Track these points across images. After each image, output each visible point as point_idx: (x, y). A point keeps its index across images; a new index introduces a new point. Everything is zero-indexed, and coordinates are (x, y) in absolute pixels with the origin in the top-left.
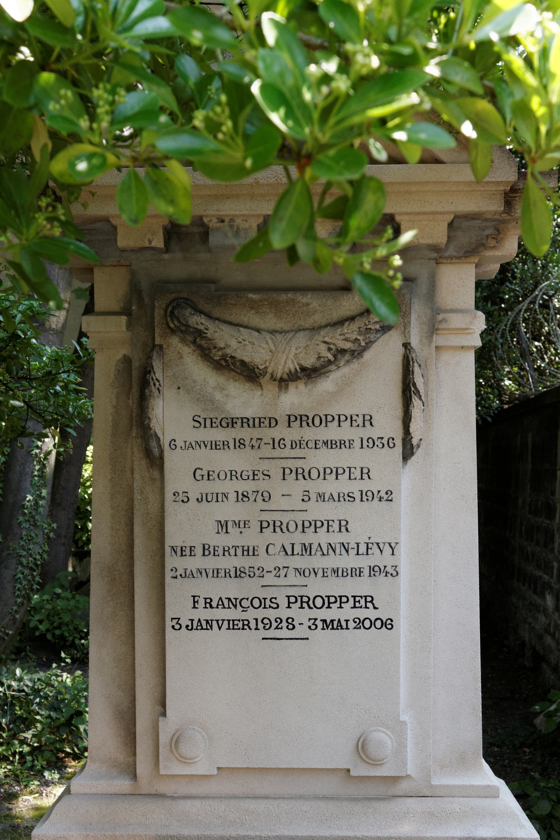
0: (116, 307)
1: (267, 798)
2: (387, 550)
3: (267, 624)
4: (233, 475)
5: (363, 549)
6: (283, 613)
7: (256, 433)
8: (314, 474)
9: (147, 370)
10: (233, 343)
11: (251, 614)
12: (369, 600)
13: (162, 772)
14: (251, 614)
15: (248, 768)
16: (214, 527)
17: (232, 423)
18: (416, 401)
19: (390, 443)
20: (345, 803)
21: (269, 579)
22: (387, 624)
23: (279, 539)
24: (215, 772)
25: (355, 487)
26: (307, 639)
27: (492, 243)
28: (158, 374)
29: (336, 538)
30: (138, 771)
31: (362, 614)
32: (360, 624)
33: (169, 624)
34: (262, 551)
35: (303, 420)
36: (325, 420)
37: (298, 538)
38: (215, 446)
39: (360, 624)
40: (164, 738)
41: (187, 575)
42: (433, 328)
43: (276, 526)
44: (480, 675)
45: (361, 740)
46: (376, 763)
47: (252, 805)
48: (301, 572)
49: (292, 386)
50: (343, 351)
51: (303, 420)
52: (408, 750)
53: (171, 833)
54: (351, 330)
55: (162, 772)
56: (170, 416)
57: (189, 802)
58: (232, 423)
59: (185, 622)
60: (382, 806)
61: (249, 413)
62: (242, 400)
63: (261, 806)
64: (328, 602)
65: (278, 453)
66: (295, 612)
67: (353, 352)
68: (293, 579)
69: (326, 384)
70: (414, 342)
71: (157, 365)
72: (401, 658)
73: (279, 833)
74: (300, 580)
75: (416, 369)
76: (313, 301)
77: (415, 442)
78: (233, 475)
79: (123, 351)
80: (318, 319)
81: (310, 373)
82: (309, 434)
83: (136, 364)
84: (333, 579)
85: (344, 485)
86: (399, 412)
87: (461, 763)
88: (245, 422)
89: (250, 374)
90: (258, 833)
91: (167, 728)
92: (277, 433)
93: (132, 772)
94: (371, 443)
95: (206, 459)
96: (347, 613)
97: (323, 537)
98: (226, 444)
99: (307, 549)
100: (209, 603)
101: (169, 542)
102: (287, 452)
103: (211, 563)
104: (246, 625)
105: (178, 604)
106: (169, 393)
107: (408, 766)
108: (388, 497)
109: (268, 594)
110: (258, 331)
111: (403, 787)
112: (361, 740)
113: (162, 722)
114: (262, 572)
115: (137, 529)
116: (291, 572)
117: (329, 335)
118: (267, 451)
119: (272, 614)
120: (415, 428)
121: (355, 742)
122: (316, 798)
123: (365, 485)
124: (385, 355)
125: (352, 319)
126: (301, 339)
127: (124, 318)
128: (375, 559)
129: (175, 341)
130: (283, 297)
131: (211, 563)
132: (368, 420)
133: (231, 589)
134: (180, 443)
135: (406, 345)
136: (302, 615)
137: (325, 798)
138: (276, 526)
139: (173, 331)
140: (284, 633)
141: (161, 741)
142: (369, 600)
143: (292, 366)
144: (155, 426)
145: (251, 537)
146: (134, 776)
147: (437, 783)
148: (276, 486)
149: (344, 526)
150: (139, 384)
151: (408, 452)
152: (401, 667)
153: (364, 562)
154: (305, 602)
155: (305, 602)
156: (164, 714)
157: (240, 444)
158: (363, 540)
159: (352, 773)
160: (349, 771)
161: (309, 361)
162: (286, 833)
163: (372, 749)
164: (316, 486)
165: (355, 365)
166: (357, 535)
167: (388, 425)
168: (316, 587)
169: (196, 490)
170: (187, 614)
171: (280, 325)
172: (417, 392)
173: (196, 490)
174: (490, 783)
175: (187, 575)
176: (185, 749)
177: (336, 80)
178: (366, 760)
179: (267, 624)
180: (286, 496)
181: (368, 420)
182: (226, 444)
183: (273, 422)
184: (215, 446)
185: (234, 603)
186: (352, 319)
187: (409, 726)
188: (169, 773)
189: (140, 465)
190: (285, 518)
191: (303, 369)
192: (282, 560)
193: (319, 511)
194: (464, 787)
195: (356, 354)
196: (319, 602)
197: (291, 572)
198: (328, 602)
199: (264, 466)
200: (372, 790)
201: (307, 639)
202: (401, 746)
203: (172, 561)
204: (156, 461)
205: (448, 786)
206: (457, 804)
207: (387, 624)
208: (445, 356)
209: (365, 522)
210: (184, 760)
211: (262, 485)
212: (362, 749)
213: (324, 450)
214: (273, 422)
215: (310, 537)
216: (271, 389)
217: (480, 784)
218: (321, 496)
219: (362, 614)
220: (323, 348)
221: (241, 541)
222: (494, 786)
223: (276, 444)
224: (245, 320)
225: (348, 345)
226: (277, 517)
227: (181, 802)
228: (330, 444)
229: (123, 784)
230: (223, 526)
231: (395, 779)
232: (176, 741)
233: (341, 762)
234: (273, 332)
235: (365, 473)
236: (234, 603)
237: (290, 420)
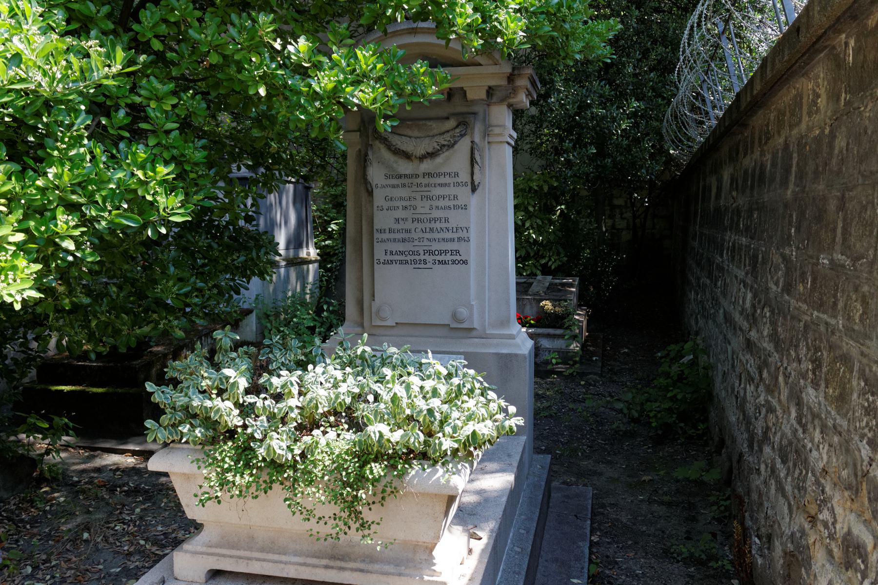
0: (356, 128)
2: (465, 230)
3: (415, 262)
4: (401, 199)
5: (455, 230)
6: (422, 257)
7: (410, 181)
8: (434, 198)
9: (366, 155)
10: (399, 143)
11: (409, 258)
12: (458, 252)
14: (409, 258)
16: (393, 221)
17: (400, 176)
18: (476, 166)
19: (466, 184)
21: (416, 243)
22: (465, 262)
23: (420, 226)
25: (451, 203)
27: (512, 95)
28: (370, 156)
29: (444, 225)
31: (454, 258)
32: (454, 262)
33: (375, 262)
34: (413, 231)
35: (430, 175)
36: (439, 175)
37: (428, 225)
38: (393, 186)
39: (454, 262)
40: (374, 310)
41: (383, 241)
42: (486, 134)
43: (418, 220)
48: (429, 240)
49: (425, 161)
50: (444, 145)
51: (430, 175)
54: (447, 136)
56: (376, 175)
58: (400, 176)
59: (382, 261)
61: (407, 172)
62: (405, 167)
64: (440, 253)
65: (418, 189)
66: (427, 257)
67: (448, 146)
68: (426, 243)
69: (439, 160)
70: (477, 139)
71: (370, 153)
74: (429, 243)
75: (476, 152)
76: (433, 124)
77: (476, 183)
78: (401, 199)
79: (359, 147)
80: (435, 132)
81: (432, 155)
82: (432, 181)
83: (363, 153)
84: (443, 243)
85: (446, 203)
86: (469, 171)
88: (406, 176)
89: (407, 156)
92: (419, 180)
94: (458, 184)
95: (389, 192)
96: (449, 257)
97: (438, 225)
98: (398, 186)
99: (431, 230)
100: (391, 253)
101: (375, 227)
102: (423, 189)
103: (392, 236)
104: (407, 262)
105: (379, 254)
106: (375, 164)
108: (465, 207)
109: (416, 249)
110: (410, 137)
111: (474, 333)
113: (373, 303)
114: (413, 240)
115: (364, 222)
116: (425, 240)
117: (437, 139)
118: (415, 188)
119: (417, 258)
120: (477, 178)
123: (456, 202)
124: (464, 146)
125: (448, 131)
126: (427, 141)
127: (358, 133)
128: (460, 234)
129: (377, 142)
130: (421, 123)
131: (392, 236)
132: (457, 175)
133: (401, 247)
134: (379, 185)
135: (472, 142)
136: (430, 258)
138: (418, 220)
139: (376, 138)
140: (422, 266)
142: (458, 252)
143: (423, 152)
144: (369, 178)
145: (408, 225)
148: (419, 203)
149: (447, 220)
150: (363, 161)
151: (474, 190)
153: (455, 236)
154: (431, 253)
155: (431, 253)
157: (404, 185)
158: (455, 226)
161: (430, 150)
164: (435, 203)
165: (451, 151)
166: (453, 224)
167: (465, 177)
168: (436, 246)
169: (386, 205)
170: (383, 258)
171: (419, 135)
172: (477, 162)
173: (386, 205)
175: (383, 241)
179: (415, 262)
180: (423, 207)
181: (457, 175)
182: (398, 186)
183: (417, 176)
184: (393, 186)
185: (402, 253)
186: (448, 131)
189: (364, 195)
190: (422, 217)
191: (428, 153)
192: (421, 235)
193: (436, 214)
195: (451, 146)
196: (437, 253)
197: (425, 240)
198: (440, 253)
199: (413, 195)
203: (377, 235)
204: (370, 193)
206: (495, 341)
207: (465, 262)
208: (494, 146)
209: (455, 218)
210: (383, 319)
211: (413, 203)
212: (454, 316)
213: (438, 188)
214: (417, 176)
215: (433, 225)
216: (416, 162)
218: (437, 207)
219: (454, 258)
220: (435, 144)
221: (405, 227)
223: (418, 185)
224: (405, 133)
225: (446, 143)
226: (419, 216)
228: (441, 185)
230: (397, 220)
232: (378, 311)
234: (416, 138)
235: (455, 197)
236: (402, 253)
237: (424, 175)
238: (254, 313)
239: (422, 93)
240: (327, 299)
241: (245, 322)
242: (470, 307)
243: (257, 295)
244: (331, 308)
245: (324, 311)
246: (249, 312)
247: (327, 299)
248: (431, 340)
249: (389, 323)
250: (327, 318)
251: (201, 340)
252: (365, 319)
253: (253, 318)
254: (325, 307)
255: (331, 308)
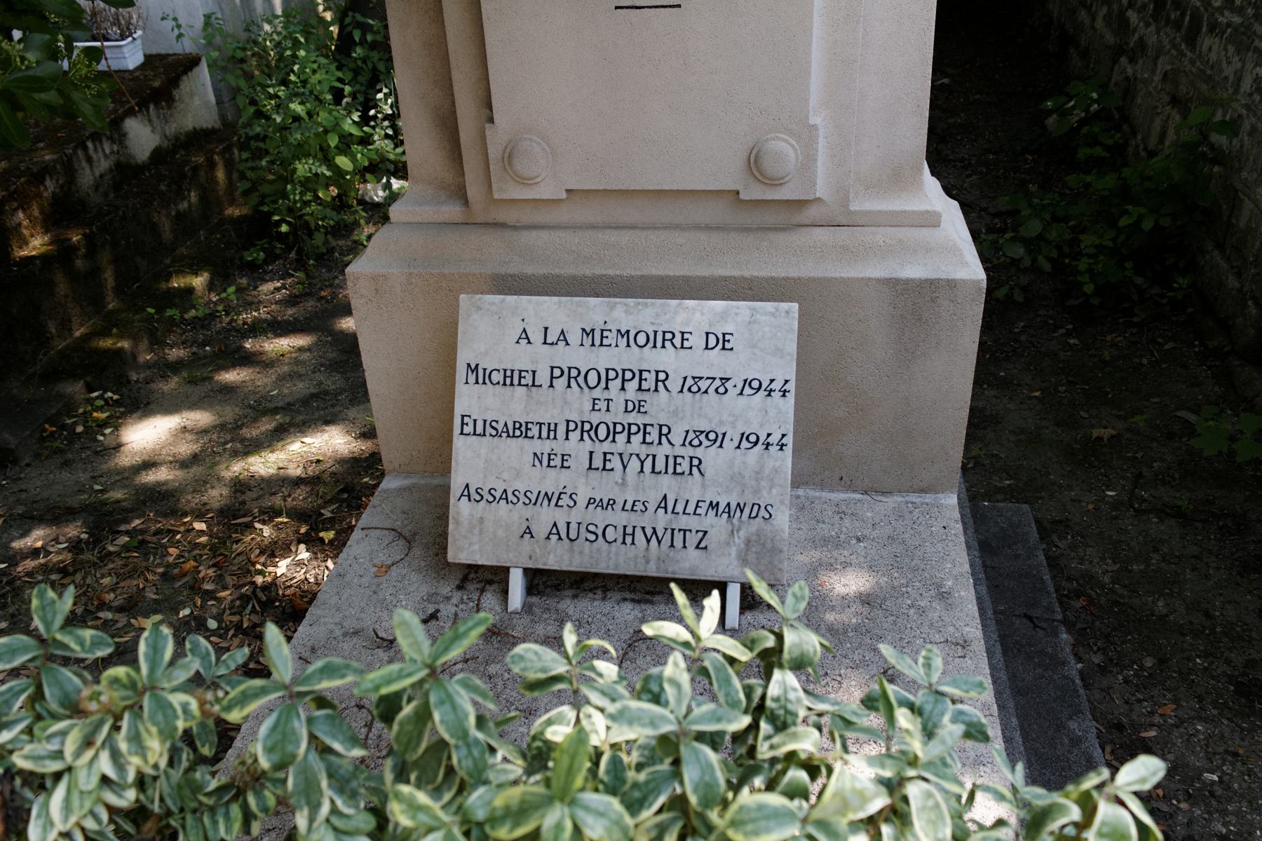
1: (633, 227)
13: (496, 196)
15: (605, 190)
20: (733, 235)
24: (564, 195)
26: (679, 6)
30: (469, 194)
40: (494, 152)
44: (931, 55)
45: (754, 152)
46: (774, 182)
47: (612, 237)
52: (819, 163)
53: (511, 271)
55: (496, 196)
57: (534, 233)
60: (781, 238)
63: (624, 237)
72: (815, 31)
73: (645, 272)
87: (898, 180)
90: (618, 272)
91: (497, 138)
93: (460, 194)
107: (818, 187)
111: (812, 213)
112: (754, 152)
121: (746, 155)
122: (698, 227)
137: (708, 228)
141: (491, 156)
146: (466, 202)
147: (857, 208)
152: (814, 45)
156: (491, 120)
159: (742, 196)
160: (738, 193)
162: (654, 272)
163: (769, 165)
174: (929, 208)
176: (521, 165)
177: (871, 780)
178: (757, 174)
187: (821, 132)
188: (506, 196)
194: (893, 213)
200: (770, 218)
201: (679, 6)
202: (809, 160)
205: (871, 212)
206: (881, 236)
210: (524, 181)
212: (755, 164)
217: (915, 209)
222: (935, 212)
227: (525, 233)
229: (452, 211)
231: (800, 204)
232: (509, 157)
233: (726, 183)
238: (204, 65)
239: (106, 557)
240: (359, 17)
241: (186, 84)
242: (806, 136)
243: (208, 17)
244: (369, 38)
245: (355, 44)
246: (190, 63)
247: (359, 17)
248: (680, 238)
249: (545, 191)
250: (364, 61)
251: (85, 149)
252: (469, 177)
253: (203, 74)
254: (357, 35)
255: (369, 38)
